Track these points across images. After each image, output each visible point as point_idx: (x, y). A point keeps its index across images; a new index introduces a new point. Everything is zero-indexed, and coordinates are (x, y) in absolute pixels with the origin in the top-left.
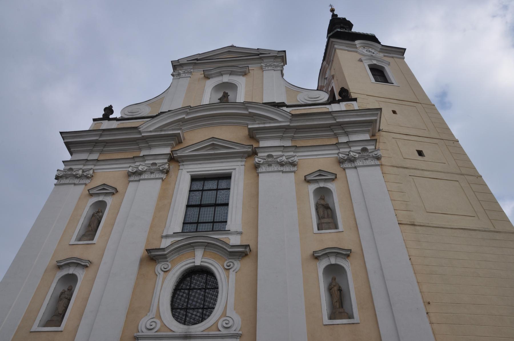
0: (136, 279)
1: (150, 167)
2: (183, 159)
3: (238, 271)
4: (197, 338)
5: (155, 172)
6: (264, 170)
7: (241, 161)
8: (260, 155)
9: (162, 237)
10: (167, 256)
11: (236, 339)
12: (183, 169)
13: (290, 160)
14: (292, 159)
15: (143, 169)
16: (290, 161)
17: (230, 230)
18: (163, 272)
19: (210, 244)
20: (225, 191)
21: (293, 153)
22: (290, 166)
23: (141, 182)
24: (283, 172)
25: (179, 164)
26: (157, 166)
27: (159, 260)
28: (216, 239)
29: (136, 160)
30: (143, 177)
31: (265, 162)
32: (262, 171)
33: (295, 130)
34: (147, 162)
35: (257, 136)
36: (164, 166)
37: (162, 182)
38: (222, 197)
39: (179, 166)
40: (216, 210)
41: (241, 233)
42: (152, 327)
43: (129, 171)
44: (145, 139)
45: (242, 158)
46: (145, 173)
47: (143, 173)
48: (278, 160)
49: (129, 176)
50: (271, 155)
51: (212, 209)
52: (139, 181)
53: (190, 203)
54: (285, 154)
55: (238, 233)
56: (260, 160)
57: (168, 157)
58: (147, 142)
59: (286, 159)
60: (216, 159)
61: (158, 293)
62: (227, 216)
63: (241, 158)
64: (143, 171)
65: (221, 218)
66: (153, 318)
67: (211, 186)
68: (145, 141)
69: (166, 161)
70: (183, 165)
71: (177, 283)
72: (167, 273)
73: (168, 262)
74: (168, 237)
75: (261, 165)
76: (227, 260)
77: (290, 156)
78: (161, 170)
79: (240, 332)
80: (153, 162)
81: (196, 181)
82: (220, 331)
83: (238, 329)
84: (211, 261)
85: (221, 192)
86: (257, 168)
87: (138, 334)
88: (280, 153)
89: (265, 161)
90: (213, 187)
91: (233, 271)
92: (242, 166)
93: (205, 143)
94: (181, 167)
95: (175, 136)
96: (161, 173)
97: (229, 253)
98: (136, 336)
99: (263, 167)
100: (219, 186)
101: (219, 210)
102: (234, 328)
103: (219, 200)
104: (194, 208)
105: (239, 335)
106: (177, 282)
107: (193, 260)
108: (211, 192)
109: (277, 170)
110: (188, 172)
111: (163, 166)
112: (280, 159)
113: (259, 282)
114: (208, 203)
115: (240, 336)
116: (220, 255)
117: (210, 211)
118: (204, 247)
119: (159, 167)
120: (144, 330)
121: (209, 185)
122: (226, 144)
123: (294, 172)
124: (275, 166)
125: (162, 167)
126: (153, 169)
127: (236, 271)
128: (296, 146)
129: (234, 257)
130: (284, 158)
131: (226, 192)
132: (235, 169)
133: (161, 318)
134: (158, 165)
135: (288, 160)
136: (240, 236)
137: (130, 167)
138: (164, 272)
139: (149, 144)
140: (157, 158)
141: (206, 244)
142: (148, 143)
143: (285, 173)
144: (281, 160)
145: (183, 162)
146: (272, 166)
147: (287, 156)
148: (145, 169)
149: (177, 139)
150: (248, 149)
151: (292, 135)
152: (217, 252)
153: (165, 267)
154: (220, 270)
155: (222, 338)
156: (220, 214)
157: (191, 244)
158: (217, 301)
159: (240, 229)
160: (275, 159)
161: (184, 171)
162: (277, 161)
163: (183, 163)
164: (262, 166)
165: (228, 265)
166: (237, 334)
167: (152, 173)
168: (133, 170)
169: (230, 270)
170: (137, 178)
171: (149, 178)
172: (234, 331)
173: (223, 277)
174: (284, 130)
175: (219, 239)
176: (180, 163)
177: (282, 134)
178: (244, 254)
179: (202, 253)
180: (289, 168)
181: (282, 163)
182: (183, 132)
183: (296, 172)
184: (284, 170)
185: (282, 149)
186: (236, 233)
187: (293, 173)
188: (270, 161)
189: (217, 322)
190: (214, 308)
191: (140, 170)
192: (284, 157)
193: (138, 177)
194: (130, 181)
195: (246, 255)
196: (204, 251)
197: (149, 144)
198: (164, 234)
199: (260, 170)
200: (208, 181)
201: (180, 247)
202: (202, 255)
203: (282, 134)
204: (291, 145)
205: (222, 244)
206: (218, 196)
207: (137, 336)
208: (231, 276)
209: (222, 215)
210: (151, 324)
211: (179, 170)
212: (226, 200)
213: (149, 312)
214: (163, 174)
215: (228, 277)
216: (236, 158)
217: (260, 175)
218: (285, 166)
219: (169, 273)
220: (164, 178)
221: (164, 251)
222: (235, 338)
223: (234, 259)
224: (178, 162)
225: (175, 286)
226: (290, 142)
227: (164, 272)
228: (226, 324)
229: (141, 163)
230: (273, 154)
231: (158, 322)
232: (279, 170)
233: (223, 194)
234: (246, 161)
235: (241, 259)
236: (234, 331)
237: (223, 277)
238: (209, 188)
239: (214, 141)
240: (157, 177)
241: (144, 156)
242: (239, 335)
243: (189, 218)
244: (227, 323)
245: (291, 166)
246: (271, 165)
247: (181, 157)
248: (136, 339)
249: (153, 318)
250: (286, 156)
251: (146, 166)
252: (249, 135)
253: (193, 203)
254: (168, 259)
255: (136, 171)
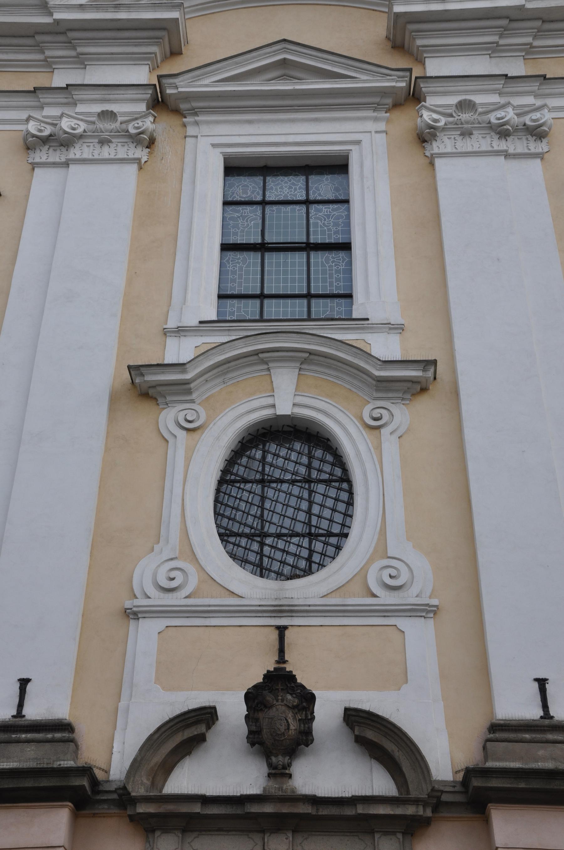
0: (105, 451)
1: (94, 123)
2: (195, 104)
3: (404, 434)
4: (312, 614)
5: (113, 140)
6: (449, 149)
7: (376, 119)
8: (431, 101)
9: (166, 333)
10: (192, 385)
11: (423, 618)
12: (199, 137)
13: (527, 120)
14: (536, 115)
15: (74, 129)
16: (529, 123)
17: (368, 319)
18: (184, 432)
19: (315, 355)
20: (331, 206)
21: (532, 97)
22: (527, 139)
23: (73, 168)
24: (507, 155)
25: (184, 120)
26: (118, 123)
27: (169, 398)
28: (341, 341)
29: (45, 98)
30: (75, 152)
31: (451, 123)
32: (442, 150)
33: (538, 23)
34: (81, 108)
35: (419, 42)
36: (141, 124)
37: (138, 171)
38: (324, 224)
39: (184, 126)
40: (312, 260)
41: (399, 328)
42: (174, 584)
43: (28, 133)
44: (64, 33)
45: (375, 110)
46: (81, 141)
47: (74, 142)
48: (493, 118)
49: (28, 149)
50: (470, 101)
51: (299, 258)
52: (66, 164)
53: (232, 240)
54: (512, 102)
55: (390, 329)
56: (435, 116)
57: (148, 94)
58: (71, 43)
59: (516, 117)
60: (297, 111)
61: (178, 490)
62: (350, 280)
63: (374, 111)
64: (74, 136)
65: (331, 284)
66: (172, 559)
67: (286, 191)
68: (62, 38)
69: (142, 107)
70: (197, 123)
71: (226, 462)
72: (196, 435)
73: (194, 402)
74: (182, 334)
75: (438, 134)
76: (369, 402)
77: (527, 109)
78: (131, 136)
79: (435, 602)
80: (104, 109)
81: (239, 175)
82: (375, 596)
83: (428, 593)
84: (323, 403)
85: (320, 211)
86: (424, 141)
87: (137, 602)
88: (494, 98)
89: (451, 119)
90: (295, 195)
91: (391, 433)
92: (378, 135)
93: (254, 58)
94: (191, 130)
95: (164, 29)
96: (132, 146)
97: (374, 383)
98: (131, 609)
99: (445, 139)
100: (311, 192)
101: (322, 262)
102: (414, 590)
103: (315, 232)
104: (245, 254)
105: (432, 609)
106: (226, 460)
107: (270, 401)
108: (289, 208)
109: (490, 149)
110: (214, 146)
111: (139, 121)
112: (499, 116)
113: (471, 466)
114: (285, 241)
115: (435, 613)
116: (348, 387)
117: (293, 264)
118: (298, 365)
119: (124, 126)
120: (151, 591)
121: (282, 188)
122: (325, 63)
123: (540, 156)
124: (483, 137)
125: (136, 125)
126: (107, 131)
127: (399, 433)
128: (544, 77)
129: (390, 395)
130: (510, 114)
131: (333, 210)
132: (358, 142)
133: (197, 559)
134: (120, 119)
135: (522, 120)
136: (399, 335)
137: (28, 120)
138: (188, 430)
139: (79, 50)
140: (111, 97)
141: (306, 355)
142: (74, 48)
143: (514, 158)
144: (502, 118)
145: (196, 114)
146: (472, 136)
147: (519, 106)
148: (79, 131)
149: (166, 39)
150: (397, 81)
151: (529, 40)
152: (337, 377)
153: (189, 418)
154: (352, 429)
155: (384, 616)
156: (324, 272)
157: (261, 355)
158: (351, 516)
159: (396, 318)
160: (480, 114)
161: (204, 143)
162: (489, 122)
163: (197, 118)
164: (442, 134)
165: (376, 414)
166: (427, 605)
167: (103, 142)
168: (40, 131)
169: (383, 431)
170: (56, 156)
171: (96, 157)
172: (417, 596)
173: (362, 448)
174: (504, 22)
175: (347, 342)
176: (185, 117)
177: (495, 38)
178: (418, 387)
179: (295, 381)
180: (525, 145)
181: (505, 127)
182: (187, 17)
183: (546, 156)
184: (511, 151)
185: (499, 84)
186: (385, 328)
187: (538, 161)
188: (467, 123)
189: (363, 573)
190: (346, 536)
191: (66, 132)
192: (510, 110)
193: (58, 152)
194: (34, 166)
195: (424, 390)
196: (299, 374)
197: (79, 50)
198: (172, 324)
199: (436, 147)
200: (277, 175)
201: (229, 362)
202: (294, 387)
203: (495, 38)
204: (523, 73)
205: (355, 355)
206: (311, 221)
207: (135, 609)
208: (385, 446)
209: (331, 276)
210: (172, 576)
211: (185, 137)
212: (336, 232)
213: (158, 542)
214: (139, 149)
215: (379, 448)
216: (358, 109)
217: (438, 162)
218: (512, 137)
219: (203, 433)
220: (143, 161)
221: (184, 371)
222: (421, 616)
223: (389, 398)
224: (177, 112)
225: (221, 471)
226: (521, 61)
227: (188, 430)
228: (391, 576)
229: (67, 110)
230: (478, 99)
231: (190, 568)
232: (496, 148)
233: (328, 216)
234: (388, 121)
235: (410, 400)
236: (417, 596)
237: (362, 448)
238: (282, 198)
239: (286, 50)
240: (122, 154)
241: (69, 87)
242: (432, 609)
243: (234, 281)
244: (392, 574)
245: (529, 137)
246: (471, 134)
247: (188, 97)
248: (131, 616)
249: (172, 559)
250: (514, 108)
251: (82, 120)
252: (388, 38)
253: (240, 240)
254: (194, 396)
255: (51, 135)
